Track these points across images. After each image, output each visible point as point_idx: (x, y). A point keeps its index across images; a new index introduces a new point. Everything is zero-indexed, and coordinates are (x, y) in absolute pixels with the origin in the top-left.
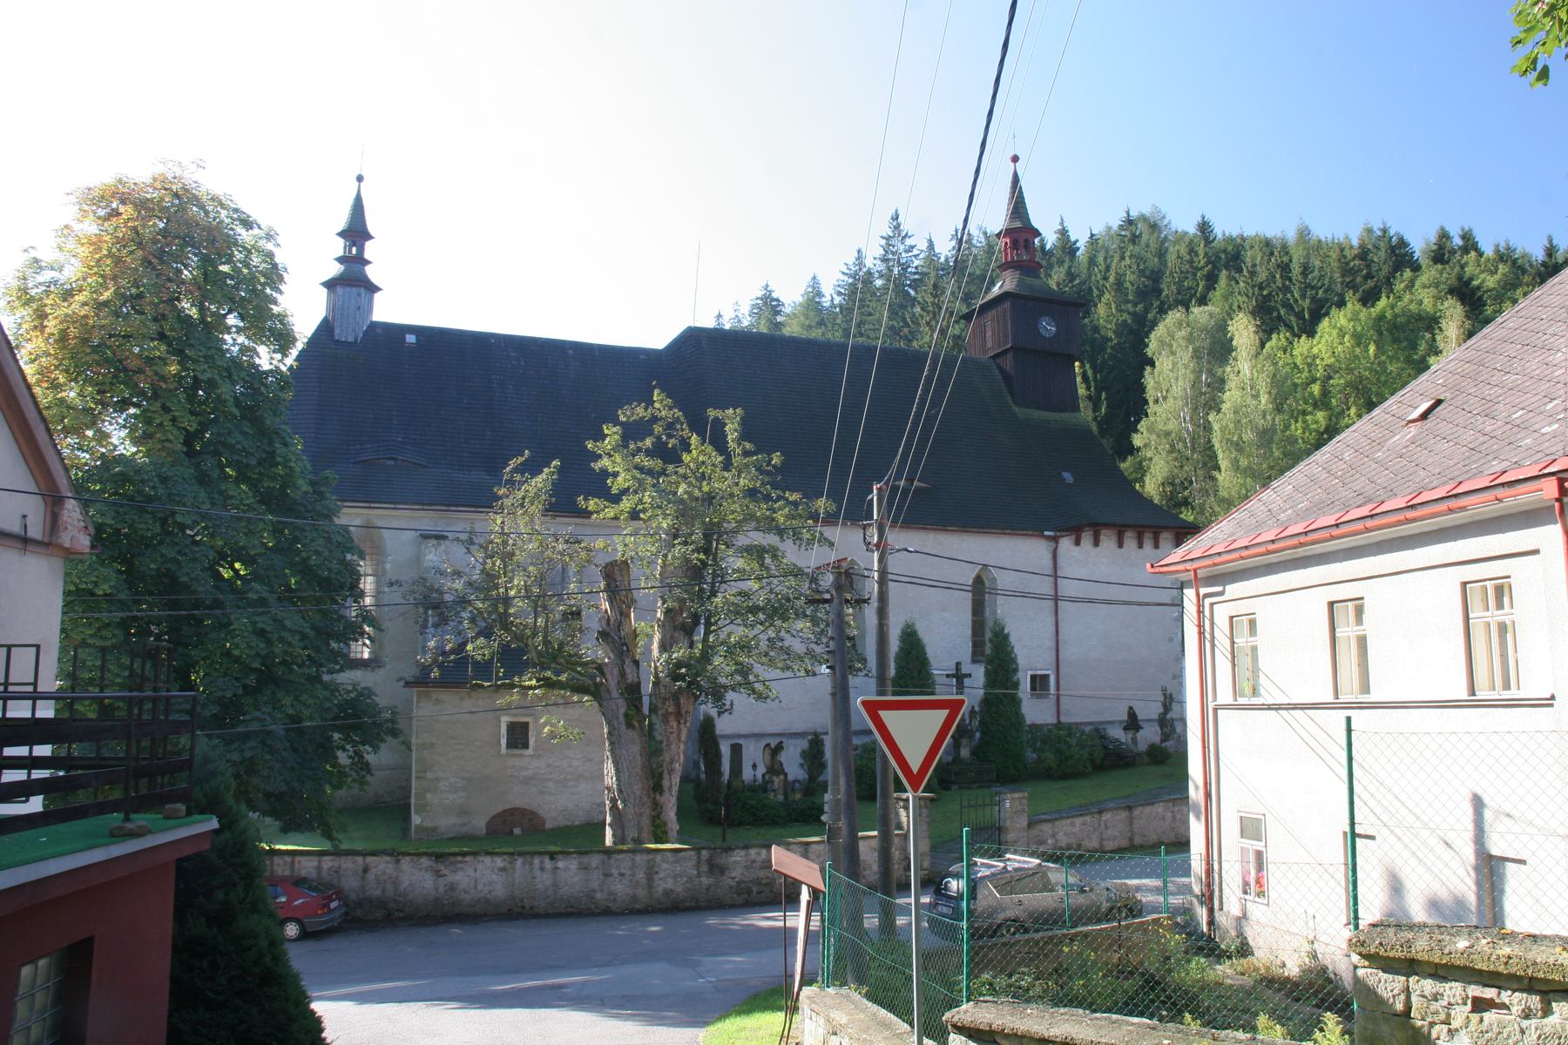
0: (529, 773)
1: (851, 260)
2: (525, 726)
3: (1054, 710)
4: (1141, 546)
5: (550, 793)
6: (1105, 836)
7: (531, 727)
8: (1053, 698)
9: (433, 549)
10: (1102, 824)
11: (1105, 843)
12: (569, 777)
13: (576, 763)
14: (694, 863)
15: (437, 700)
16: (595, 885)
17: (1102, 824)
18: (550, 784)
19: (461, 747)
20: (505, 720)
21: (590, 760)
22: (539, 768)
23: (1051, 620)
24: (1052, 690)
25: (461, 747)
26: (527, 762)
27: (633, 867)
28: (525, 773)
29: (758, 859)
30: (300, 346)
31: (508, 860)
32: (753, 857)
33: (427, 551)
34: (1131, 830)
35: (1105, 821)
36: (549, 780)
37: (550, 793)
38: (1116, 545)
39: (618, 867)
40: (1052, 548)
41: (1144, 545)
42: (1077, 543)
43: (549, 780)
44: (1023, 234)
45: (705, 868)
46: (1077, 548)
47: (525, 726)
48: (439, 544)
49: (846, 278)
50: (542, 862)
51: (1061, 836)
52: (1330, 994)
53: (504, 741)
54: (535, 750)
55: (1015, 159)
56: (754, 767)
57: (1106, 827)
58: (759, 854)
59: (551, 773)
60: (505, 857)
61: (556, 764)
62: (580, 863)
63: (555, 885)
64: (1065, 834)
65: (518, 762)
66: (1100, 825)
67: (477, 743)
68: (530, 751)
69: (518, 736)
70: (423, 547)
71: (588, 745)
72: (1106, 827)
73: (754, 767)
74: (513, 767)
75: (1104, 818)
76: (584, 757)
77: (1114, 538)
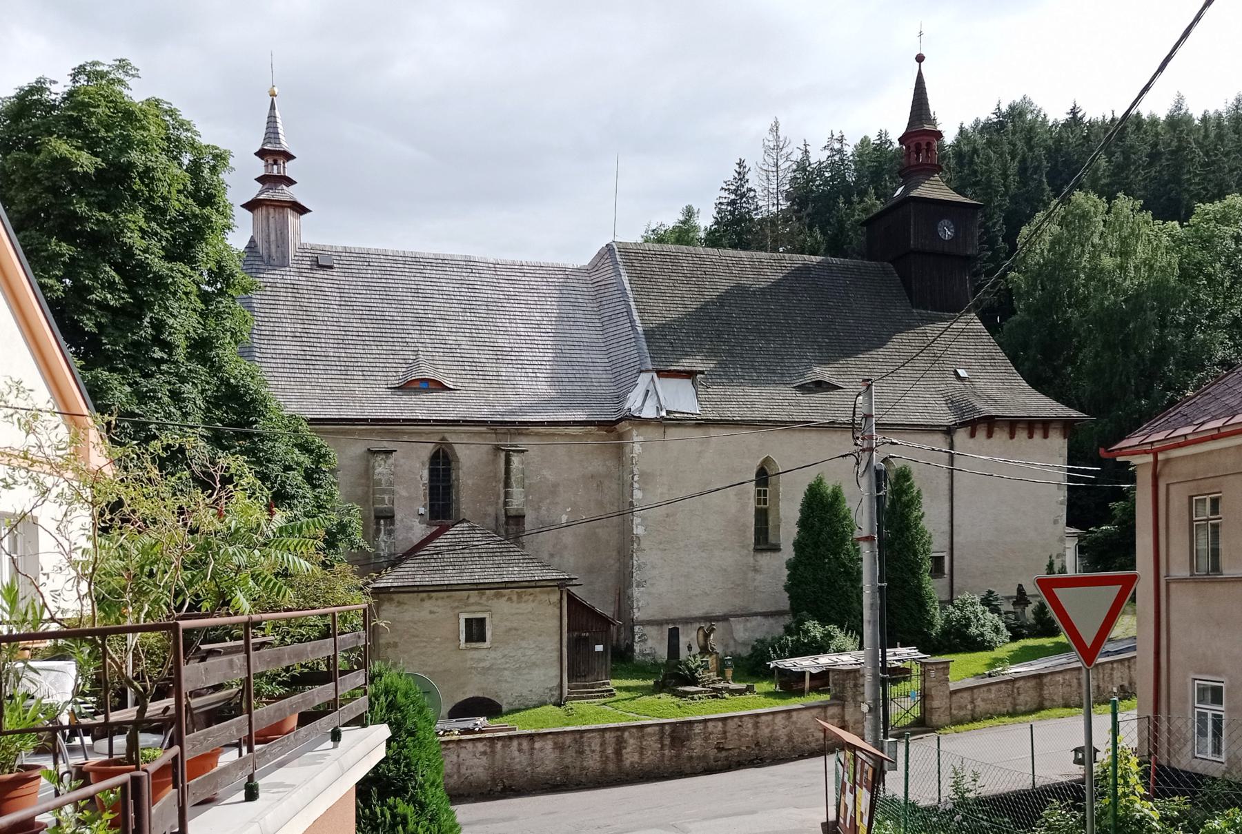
0: (487, 664)
1: (731, 175)
2: (482, 621)
3: (948, 589)
4: (1031, 437)
5: (506, 681)
6: (1018, 702)
7: (488, 622)
8: (947, 576)
9: (382, 462)
10: (1015, 690)
11: (1017, 707)
12: (523, 665)
13: (529, 653)
14: (657, 737)
15: (398, 602)
16: (568, 760)
17: (1015, 690)
18: (506, 673)
19: (422, 644)
20: (463, 617)
21: (543, 649)
22: (495, 659)
23: (947, 506)
24: (947, 570)
25: (422, 644)
26: (483, 654)
27: (603, 744)
28: (482, 665)
29: (714, 731)
30: (871, 215)
31: (488, 744)
32: (710, 730)
33: (376, 464)
34: (1041, 696)
35: (1018, 688)
36: (505, 669)
37: (506, 681)
38: (1008, 436)
39: (590, 746)
40: (949, 440)
41: (1035, 436)
42: (972, 435)
43: (505, 669)
44: (925, 138)
45: (667, 741)
46: (972, 441)
47: (482, 621)
48: (387, 458)
49: (725, 194)
50: (520, 744)
51: (979, 702)
52: (1029, 793)
53: (463, 637)
54: (491, 643)
55: (920, 59)
56: (690, 648)
57: (1019, 694)
58: (715, 727)
59: (507, 663)
60: (485, 742)
61: (511, 654)
62: (555, 743)
63: (532, 764)
64: (983, 700)
65: (476, 654)
66: (1013, 691)
67: (438, 639)
68: (487, 644)
69: (476, 630)
70: (372, 461)
71: (540, 635)
72: (1019, 694)
73: (690, 648)
74: (472, 659)
75: (1017, 685)
76: (537, 646)
77: (1007, 430)
